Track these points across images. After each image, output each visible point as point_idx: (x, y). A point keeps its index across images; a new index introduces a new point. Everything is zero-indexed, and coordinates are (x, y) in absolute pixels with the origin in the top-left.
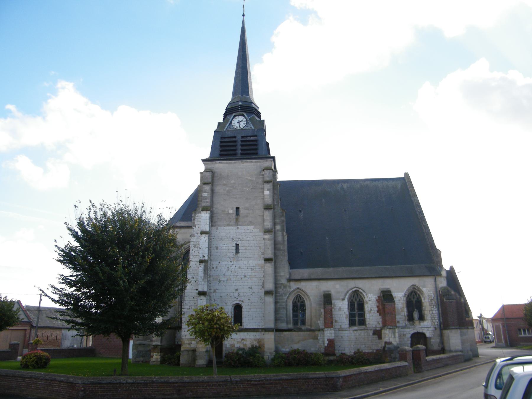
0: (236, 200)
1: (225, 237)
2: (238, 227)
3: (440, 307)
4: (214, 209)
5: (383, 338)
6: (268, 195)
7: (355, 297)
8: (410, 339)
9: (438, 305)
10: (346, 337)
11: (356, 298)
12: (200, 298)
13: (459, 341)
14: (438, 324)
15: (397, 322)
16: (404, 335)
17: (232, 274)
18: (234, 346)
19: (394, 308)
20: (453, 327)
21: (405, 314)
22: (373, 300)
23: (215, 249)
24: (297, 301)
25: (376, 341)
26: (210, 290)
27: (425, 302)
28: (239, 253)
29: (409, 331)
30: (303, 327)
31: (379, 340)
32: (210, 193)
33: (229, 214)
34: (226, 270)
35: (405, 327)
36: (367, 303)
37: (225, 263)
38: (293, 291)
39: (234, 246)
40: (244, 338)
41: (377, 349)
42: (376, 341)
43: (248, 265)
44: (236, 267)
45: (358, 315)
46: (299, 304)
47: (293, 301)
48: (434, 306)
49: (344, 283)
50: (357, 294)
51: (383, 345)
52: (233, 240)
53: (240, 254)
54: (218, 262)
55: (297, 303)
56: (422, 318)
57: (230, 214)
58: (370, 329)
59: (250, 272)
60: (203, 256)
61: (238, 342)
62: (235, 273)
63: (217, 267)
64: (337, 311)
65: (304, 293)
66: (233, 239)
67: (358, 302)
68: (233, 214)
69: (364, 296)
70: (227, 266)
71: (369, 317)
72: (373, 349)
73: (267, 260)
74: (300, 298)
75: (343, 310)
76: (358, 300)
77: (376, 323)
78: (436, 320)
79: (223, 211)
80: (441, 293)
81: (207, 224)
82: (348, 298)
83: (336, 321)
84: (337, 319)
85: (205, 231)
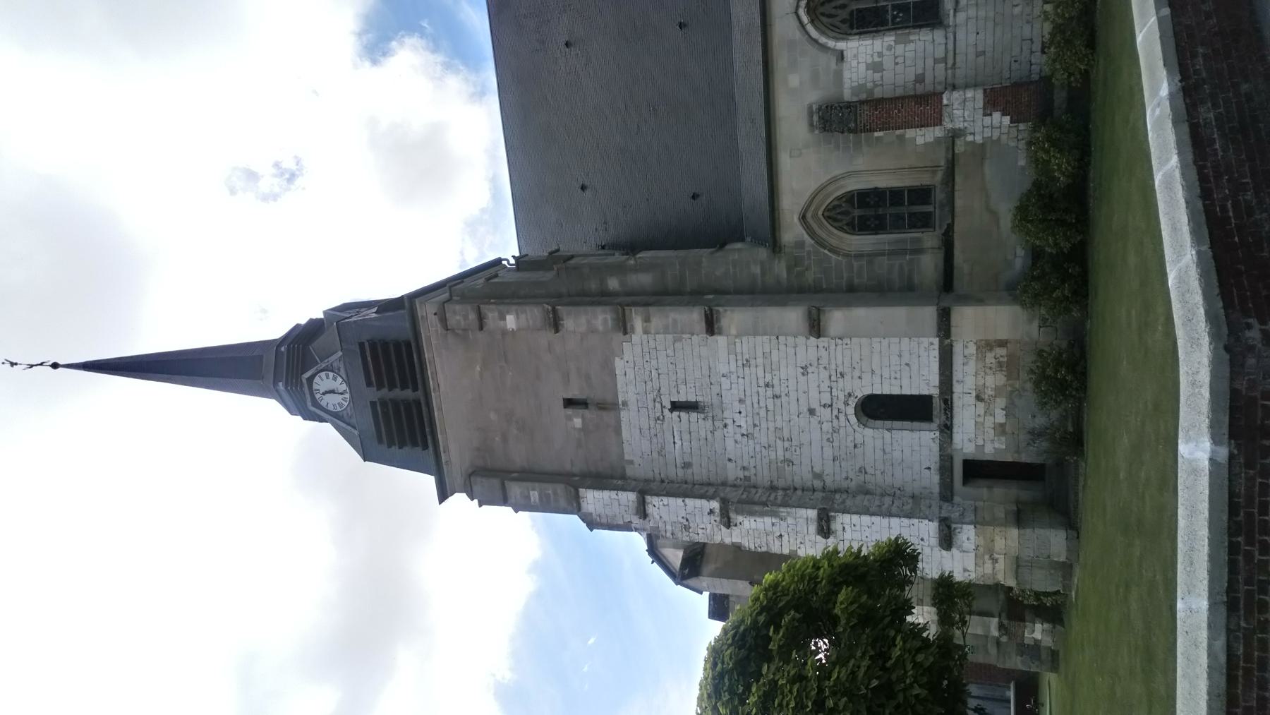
1: (654, 440)
2: (620, 403)
7: (833, 12)
30: (939, 196)
43: (734, 377)
46: (857, 213)
49: (781, 60)
64: (882, 77)
70: (738, 437)
75: (880, 54)
83: (920, 79)
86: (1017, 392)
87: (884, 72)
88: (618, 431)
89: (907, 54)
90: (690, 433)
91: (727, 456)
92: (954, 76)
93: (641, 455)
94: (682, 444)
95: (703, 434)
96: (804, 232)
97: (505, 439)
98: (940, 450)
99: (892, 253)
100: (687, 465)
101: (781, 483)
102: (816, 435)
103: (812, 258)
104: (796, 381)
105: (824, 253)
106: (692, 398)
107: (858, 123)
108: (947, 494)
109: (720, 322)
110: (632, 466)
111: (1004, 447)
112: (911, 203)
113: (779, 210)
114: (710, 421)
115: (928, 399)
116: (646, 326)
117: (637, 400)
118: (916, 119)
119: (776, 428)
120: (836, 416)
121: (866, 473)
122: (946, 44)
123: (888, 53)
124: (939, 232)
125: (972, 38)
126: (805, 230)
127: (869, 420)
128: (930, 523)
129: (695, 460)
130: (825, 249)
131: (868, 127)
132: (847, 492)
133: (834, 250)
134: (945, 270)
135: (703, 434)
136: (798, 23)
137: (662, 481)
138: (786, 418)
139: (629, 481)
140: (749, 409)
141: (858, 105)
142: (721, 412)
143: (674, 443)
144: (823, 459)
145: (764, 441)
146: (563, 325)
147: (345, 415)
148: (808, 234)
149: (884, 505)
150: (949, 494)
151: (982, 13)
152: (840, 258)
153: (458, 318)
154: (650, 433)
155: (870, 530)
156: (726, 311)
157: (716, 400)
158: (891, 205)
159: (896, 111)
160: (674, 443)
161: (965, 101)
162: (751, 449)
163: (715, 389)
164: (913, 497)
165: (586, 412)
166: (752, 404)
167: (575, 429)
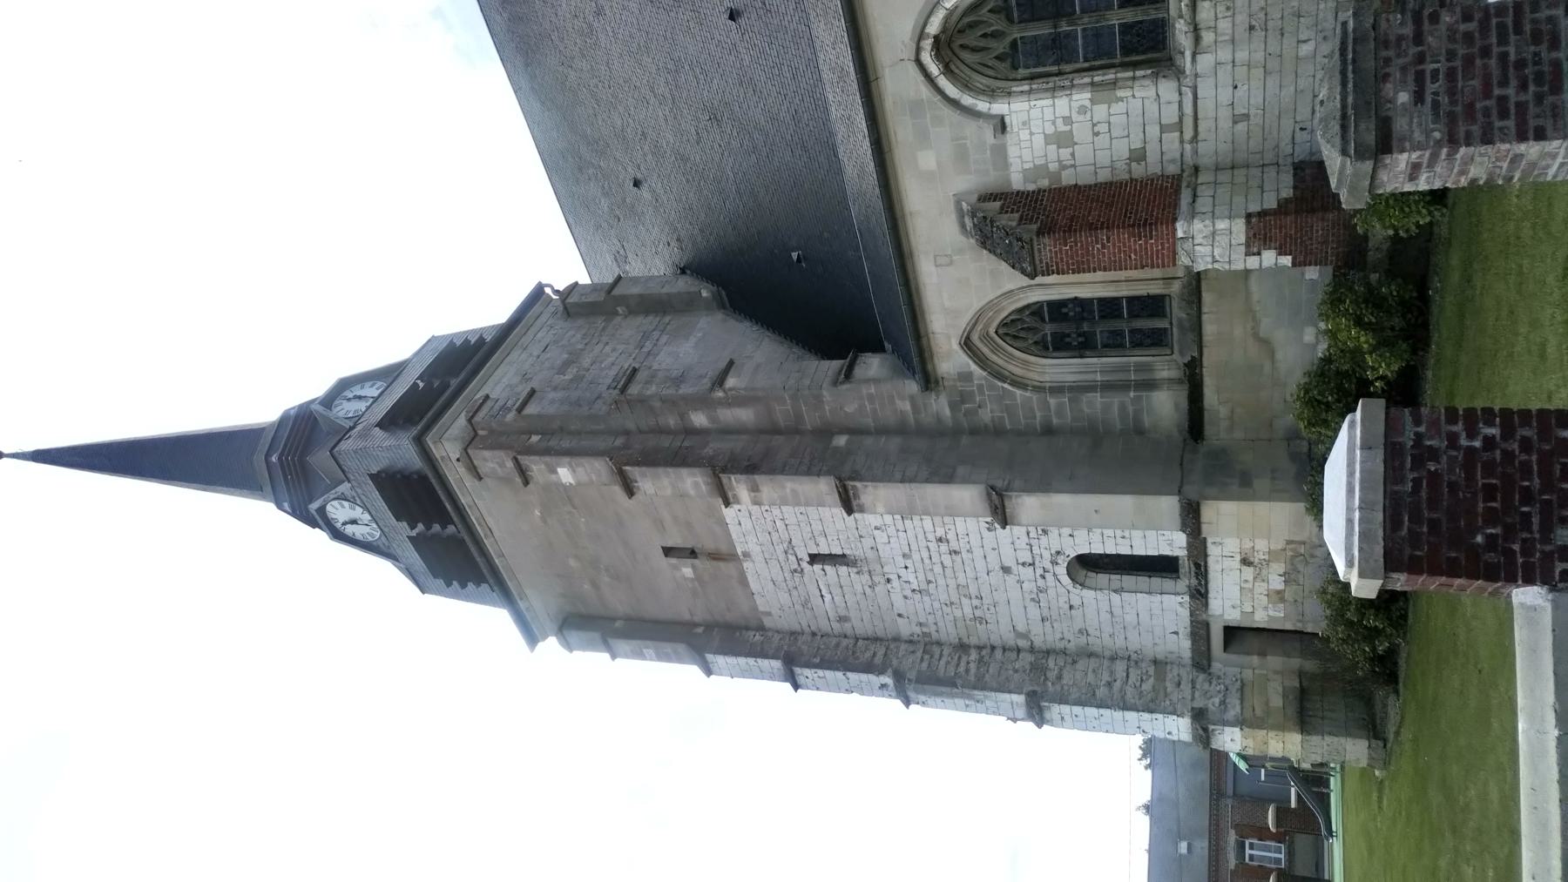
1: (795, 593)
2: (740, 554)
7: (982, 43)
10: (1239, 93)
11: (985, 36)
24: (1032, 338)
28: (844, 556)
30: (1177, 311)
40: (1238, 558)
43: (892, 531)
46: (1048, 329)
49: (901, 131)
54: (899, 619)
64: (1073, 155)
67: (1010, 20)
68: (693, 567)
70: (908, 593)
75: (1068, 120)
76: (998, 24)
83: (1139, 156)
84: (1122, 150)
86: (1302, 557)
87: (1076, 147)
88: (744, 581)
89: (1112, 119)
90: (841, 587)
91: (896, 612)
92: (1196, 152)
93: (780, 606)
94: (833, 598)
95: (859, 588)
96: (971, 362)
97: (595, 585)
98: (1191, 615)
99: (1107, 387)
100: (842, 619)
101: (973, 641)
102: (1015, 594)
103: (986, 393)
104: (979, 535)
105: (1003, 387)
106: (837, 551)
107: (1037, 262)
108: (1202, 661)
109: (859, 499)
110: (770, 618)
111: (1282, 615)
112: (1133, 315)
113: (927, 335)
114: (867, 576)
115: (1176, 559)
116: (755, 497)
117: (763, 552)
118: (1133, 256)
119: (958, 586)
120: (1041, 575)
121: (1088, 635)
122: (1180, 103)
123: (1081, 118)
124: (1180, 359)
125: (1225, 95)
126: (971, 357)
127: (1090, 574)
128: (1180, 719)
129: (853, 614)
130: (1005, 382)
131: (1055, 268)
132: (1065, 653)
133: (1018, 383)
134: (1191, 411)
135: (859, 588)
136: (921, 78)
137: (814, 634)
138: (970, 574)
139: (770, 634)
140: (919, 565)
141: (1035, 238)
142: (880, 566)
143: (822, 596)
144: (1027, 619)
145: (944, 598)
146: (638, 488)
147: (381, 546)
148: (975, 362)
149: (1115, 681)
150: (1205, 662)
151: (1242, 55)
152: (1028, 394)
153: (491, 465)
154: (787, 586)
155: (1098, 721)
156: (866, 486)
157: (870, 555)
158: (1102, 317)
159: (1099, 246)
160: (822, 596)
161: (1214, 233)
162: (928, 607)
163: (868, 542)
164: (1155, 662)
165: (696, 561)
166: (922, 559)
167: (686, 579)
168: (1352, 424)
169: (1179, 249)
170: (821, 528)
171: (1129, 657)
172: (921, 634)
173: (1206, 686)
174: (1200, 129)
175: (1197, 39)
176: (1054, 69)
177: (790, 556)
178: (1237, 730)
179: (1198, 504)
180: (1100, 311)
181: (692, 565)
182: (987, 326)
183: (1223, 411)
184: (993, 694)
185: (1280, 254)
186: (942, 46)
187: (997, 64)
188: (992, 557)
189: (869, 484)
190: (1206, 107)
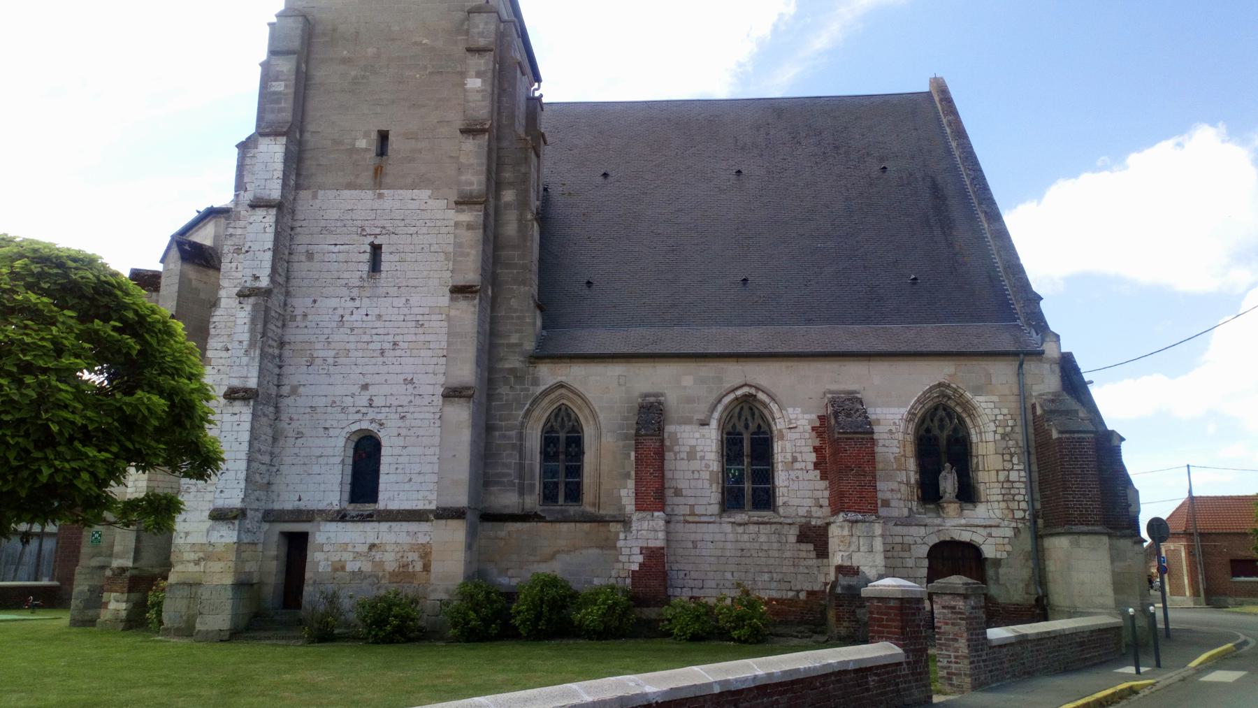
0: (378, 110)
1: (339, 224)
2: (382, 191)
3: (1034, 459)
4: (307, 136)
5: (830, 555)
6: (477, 91)
7: (743, 418)
8: (926, 563)
9: (1029, 453)
12: (230, 410)
13: (1107, 578)
14: (1027, 517)
15: (879, 502)
16: (906, 548)
17: (352, 338)
18: (343, 568)
19: (873, 454)
20: (1085, 528)
21: (908, 477)
22: (801, 429)
23: (303, 258)
24: (557, 426)
25: (809, 562)
26: (278, 386)
27: (982, 441)
29: (922, 537)
30: (572, 509)
31: (820, 560)
32: (293, 82)
33: (353, 150)
34: (334, 324)
35: (906, 522)
36: (782, 437)
37: (333, 302)
38: (546, 393)
39: (365, 252)
40: (377, 542)
41: (810, 589)
42: (809, 562)
43: (406, 311)
44: (367, 315)
45: (750, 475)
46: (562, 435)
47: (545, 425)
48: (1012, 455)
49: (707, 370)
50: (751, 409)
51: (832, 577)
52: (365, 233)
53: (383, 275)
55: (557, 432)
56: (968, 494)
57: (358, 151)
58: (789, 521)
59: (413, 330)
60: (254, 275)
61: (357, 556)
62: (365, 333)
63: (305, 315)
64: (683, 459)
65: (579, 402)
66: (363, 230)
67: (753, 433)
68: (366, 150)
69: (771, 413)
70: (340, 312)
71: (786, 483)
72: (799, 587)
73: (460, 291)
74: (569, 415)
75: (702, 458)
76: (753, 427)
77: (809, 502)
78: (1019, 502)
79: (335, 142)
80: (1039, 412)
81: (275, 177)
82: (719, 421)
83: (678, 493)
85: (267, 197)
99: (521, 467)
101: (287, 353)
102: (339, 390)
115: (374, 499)
121: (297, 438)
124: (538, 509)
125: (708, 537)
127: (354, 444)
132: (276, 419)
133: (528, 413)
139: (293, 193)
143: (336, 245)
145: (335, 337)
151: (729, 545)
152: (520, 419)
153: (481, 26)
157: (381, 291)
168: (977, 583)
169: (648, 513)
170: (409, 259)
171: (274, 466)
172: (294, 314)
173: (256, 519)
174: (691, 524)
175: (740, 525)
176: (725, 453)
177: (379, 229)
178: (235, 540)
179: (464, 518)
180: (571, 466)
181: (370, 150)
182: (569, 399)
183: (502, 534)
184: (258, 364)
185: (640, 564)
186: (749, 398)
187: (731, 425)
188: (377, 379)
189: (477, 309)
190: (704, 527)
